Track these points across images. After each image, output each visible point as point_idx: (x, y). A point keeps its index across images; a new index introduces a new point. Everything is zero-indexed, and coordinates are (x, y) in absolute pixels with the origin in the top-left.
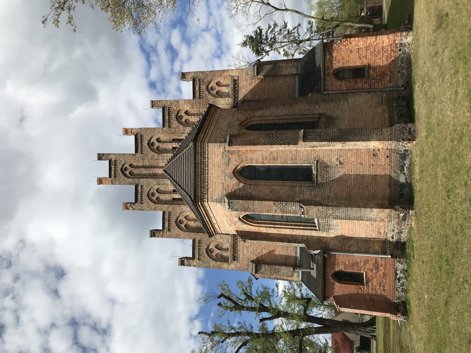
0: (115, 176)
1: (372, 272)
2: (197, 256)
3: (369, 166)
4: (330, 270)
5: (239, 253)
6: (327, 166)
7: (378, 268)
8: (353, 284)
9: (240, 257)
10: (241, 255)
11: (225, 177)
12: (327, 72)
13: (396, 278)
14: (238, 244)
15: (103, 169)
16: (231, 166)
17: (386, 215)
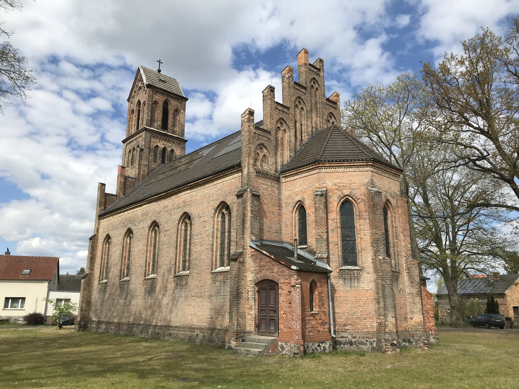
17: (391, 329)
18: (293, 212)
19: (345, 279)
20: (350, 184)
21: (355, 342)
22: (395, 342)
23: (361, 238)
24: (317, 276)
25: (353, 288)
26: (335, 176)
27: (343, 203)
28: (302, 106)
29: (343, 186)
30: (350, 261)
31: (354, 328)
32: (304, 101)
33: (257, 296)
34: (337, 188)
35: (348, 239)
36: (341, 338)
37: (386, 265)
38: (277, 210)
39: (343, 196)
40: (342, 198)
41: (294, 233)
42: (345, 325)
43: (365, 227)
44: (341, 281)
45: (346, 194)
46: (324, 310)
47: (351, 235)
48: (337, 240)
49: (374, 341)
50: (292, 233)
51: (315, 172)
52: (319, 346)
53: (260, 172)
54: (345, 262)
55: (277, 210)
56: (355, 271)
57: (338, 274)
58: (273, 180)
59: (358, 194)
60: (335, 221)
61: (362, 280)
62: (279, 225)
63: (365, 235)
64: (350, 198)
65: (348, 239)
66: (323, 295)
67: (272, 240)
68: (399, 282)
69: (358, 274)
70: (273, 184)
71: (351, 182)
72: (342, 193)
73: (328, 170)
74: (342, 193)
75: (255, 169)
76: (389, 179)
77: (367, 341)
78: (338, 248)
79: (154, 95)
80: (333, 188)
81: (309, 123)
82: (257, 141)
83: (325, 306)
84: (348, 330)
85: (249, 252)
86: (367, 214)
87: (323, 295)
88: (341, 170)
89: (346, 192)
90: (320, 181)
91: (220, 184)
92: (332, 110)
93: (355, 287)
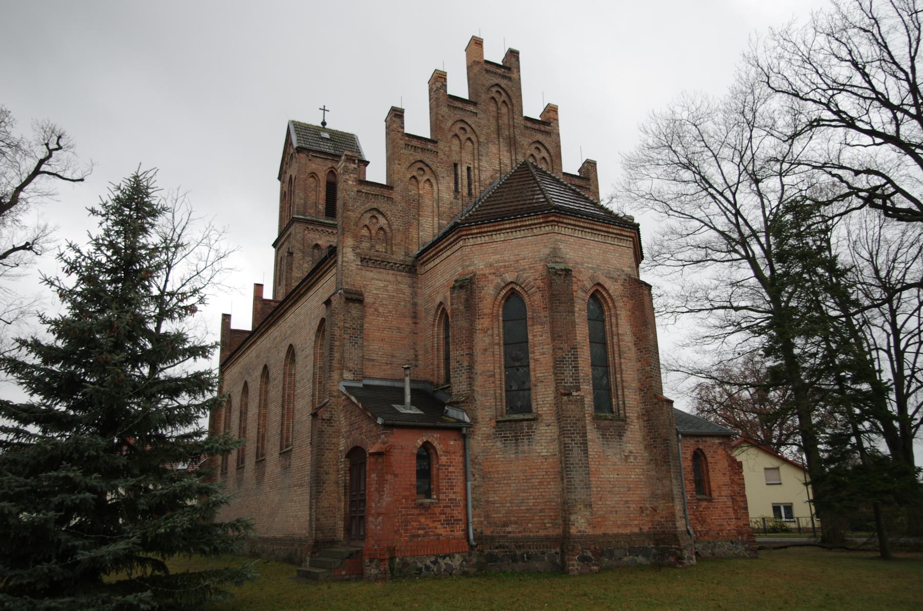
0: (487, 71)
1: (441, 514)
2: (365, 189)
3: (627, 502)
4: (436, 439)
5: (375, 270)
6: (620, 436)
7: (448, 524)
8: (708, 477)
9: (368, 273)
10: (371, 275)
11: (592, 268)
12: (699, 439)
13: (437, 556)
14: (391, 272)
15: (494, 54)
16: (607, 279)
17: (583, 529)
18: (434, 325)
19: (506, 438)
20: (517, 261)
21: (522, 556)
22: (589, 554)
23: (536, 360)
24: (437, 435)
25: (520, 455)
26: (490, 250)
27: (507, 298)
28: (468, 136)
29: (505, 266)
30: (519, 404)
31: (521, 529)
32: (473, 126)
33: (348, 478)
34: (493, 271)
35: (517, 364)
36: (497, 548)
37: (573, 407)
38: (408, 324)
39: (503, 284)
40: (503, 288)
41: (436, 362)
42: (505, 525)
43: (544, 337)
44: (498, 444)
45: (509, 280)
46: (452, 496)
47: (522, 356)
48: (492, 368)
49: (557, 553)
50: (432, 364)
51: (457, 246)
52: (435, 563)
53: (370, 260)
54: (511, 408)
55: (408, 324)
56: (525, 423)
57: (493, 430)
58: (399, 271)
59: (531, 279)
60: (490, 332)
61: (537, 437)
62: (412, 352)
63: (543, 354)
64: (518, 288)
65: (517, 364)
66: (451, 469)
67: (397, 378)
68: (624, 439)
69: (530, 427)
70: (399, 278)
71: (518, 258)
72: (503, 280)
73: (479, 241)
74: (503, 280)
75: (358, 254)
76: (604, 246)
77: (543, 553)
78: (494, 382)
79: (309, 163)
80: (487, 271)
81: (492, 164)
82: (364, 204)
83: (457, 489)
84: (510, 532)
85: (588, 419)
86: (547, 314)
87: (451, 469)
88: (502, 237)
89: (509, 277)
90: (464, 261)
91: (321, 290)
92: (540, 137)
93: (524, 452)
